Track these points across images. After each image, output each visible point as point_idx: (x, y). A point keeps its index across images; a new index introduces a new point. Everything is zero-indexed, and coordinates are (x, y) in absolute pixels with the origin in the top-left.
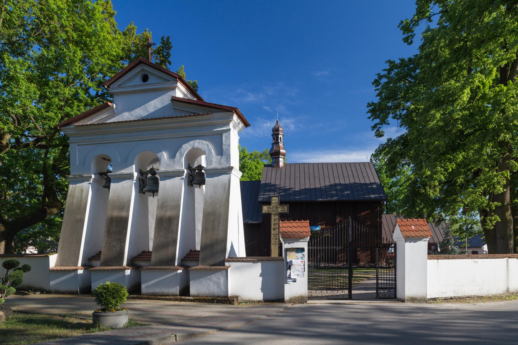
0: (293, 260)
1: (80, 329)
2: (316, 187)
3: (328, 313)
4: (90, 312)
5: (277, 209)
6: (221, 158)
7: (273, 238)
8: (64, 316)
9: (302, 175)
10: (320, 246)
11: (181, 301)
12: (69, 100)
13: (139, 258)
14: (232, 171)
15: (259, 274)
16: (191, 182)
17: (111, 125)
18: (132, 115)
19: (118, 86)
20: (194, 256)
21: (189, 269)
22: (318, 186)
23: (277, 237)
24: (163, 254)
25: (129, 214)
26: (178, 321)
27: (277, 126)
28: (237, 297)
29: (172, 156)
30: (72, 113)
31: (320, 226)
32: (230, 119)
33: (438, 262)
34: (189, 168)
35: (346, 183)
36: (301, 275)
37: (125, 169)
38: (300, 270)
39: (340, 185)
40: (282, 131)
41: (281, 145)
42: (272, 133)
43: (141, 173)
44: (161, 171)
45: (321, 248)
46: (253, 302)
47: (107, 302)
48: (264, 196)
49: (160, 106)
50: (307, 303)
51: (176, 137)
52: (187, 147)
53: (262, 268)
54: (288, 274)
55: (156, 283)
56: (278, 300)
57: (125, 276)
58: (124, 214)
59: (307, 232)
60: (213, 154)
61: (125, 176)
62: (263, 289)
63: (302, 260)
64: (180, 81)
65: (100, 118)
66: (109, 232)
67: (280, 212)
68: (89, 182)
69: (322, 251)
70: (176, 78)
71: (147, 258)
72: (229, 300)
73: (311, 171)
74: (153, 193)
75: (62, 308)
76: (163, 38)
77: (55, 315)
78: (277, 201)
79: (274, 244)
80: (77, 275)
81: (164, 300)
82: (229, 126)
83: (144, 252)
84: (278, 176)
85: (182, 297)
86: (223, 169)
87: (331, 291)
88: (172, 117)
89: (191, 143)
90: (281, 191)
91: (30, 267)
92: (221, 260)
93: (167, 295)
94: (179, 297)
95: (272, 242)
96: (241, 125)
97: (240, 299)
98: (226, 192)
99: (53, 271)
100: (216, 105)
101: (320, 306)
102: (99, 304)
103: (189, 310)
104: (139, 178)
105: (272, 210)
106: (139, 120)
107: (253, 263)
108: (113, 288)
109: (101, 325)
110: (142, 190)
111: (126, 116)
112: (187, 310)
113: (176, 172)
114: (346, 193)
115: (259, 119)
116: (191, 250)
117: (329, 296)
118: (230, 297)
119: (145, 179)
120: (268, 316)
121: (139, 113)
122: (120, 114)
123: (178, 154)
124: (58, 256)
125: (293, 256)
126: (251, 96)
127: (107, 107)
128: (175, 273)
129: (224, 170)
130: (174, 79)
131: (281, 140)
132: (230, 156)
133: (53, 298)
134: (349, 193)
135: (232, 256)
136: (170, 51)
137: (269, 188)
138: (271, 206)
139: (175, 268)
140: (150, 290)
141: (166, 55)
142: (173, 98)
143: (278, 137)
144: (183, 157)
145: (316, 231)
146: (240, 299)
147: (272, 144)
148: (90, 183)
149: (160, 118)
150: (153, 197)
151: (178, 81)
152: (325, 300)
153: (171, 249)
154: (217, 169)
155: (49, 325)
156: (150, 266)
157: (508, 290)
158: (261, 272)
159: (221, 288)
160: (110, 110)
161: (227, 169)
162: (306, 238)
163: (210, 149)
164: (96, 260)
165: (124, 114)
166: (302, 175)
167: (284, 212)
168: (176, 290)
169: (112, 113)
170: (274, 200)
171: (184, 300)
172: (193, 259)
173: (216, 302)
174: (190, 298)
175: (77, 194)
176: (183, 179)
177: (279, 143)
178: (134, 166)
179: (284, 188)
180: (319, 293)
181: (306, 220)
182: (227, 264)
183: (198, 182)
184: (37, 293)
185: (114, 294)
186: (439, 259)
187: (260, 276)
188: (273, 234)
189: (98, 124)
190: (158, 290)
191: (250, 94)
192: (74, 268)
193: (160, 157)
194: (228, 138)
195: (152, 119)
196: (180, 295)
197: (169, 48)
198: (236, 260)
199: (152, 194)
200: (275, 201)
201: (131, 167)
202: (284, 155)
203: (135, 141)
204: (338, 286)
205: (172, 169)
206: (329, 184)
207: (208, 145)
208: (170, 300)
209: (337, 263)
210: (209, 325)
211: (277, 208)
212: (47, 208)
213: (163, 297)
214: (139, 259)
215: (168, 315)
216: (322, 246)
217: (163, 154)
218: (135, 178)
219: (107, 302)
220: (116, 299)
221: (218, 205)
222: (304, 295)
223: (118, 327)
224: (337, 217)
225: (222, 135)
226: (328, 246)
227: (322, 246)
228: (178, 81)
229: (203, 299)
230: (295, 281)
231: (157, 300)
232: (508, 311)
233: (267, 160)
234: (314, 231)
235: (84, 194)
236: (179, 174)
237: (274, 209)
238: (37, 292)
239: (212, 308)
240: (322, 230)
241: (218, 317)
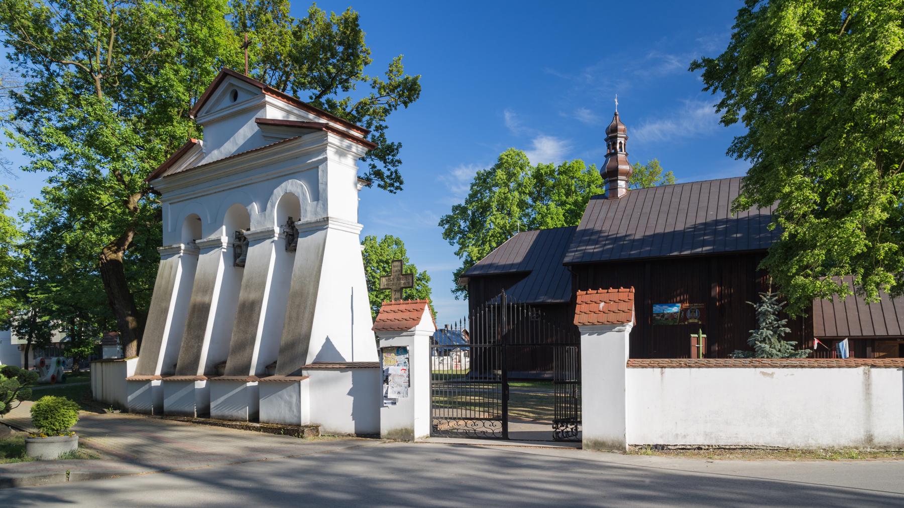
5: (398, 282)
6: (317, 204)
18: (221, 153)
19: (206, 113)
31: (679, 305)
33: (662, 373)
36: (403, 393)
37: (214, 234)
49: (249, 135)
50: (414, 442)
52: (279, 193)
55: (226, 401)
57: (194, 389)
58: (206, 299)
62: (355, 416)
63: (405, 368)
64: (269, 93)
65: (188, 163)
68: (178, 255)
80: (151, 388)
84: (611, 214)
89: (283, 185)
104: (234, 245)
105: (393, 284)
111: (216, 155)
114: (739, 235)
115: (687, 102)
121: (229, 148)
123: (269, 205)
124: (139, 361)
126: (673, 61)
127: (193, 146)
128: (244, 386)
131: (621, 148)
143: (615, 144)
145: (672, 313)
157: (870, 439)
158: (351, 386)
165: (213, 152)
166: (656, 208)
168: (245, 412)
173: (284, 434)
174: (258, 425)
178: (224, 227)
184: (115, 412)
186: (665, 367)
187: (350, 394)
191: (671, 57)
193: (251, 210)
196: (250, 421)
203: (226, 190)
207: (302, 186)
217: (253, 207)
218: (225, 245)
232: (736, 478)
234: (668, 314)
237: (396, 280)
240: (684, 311)
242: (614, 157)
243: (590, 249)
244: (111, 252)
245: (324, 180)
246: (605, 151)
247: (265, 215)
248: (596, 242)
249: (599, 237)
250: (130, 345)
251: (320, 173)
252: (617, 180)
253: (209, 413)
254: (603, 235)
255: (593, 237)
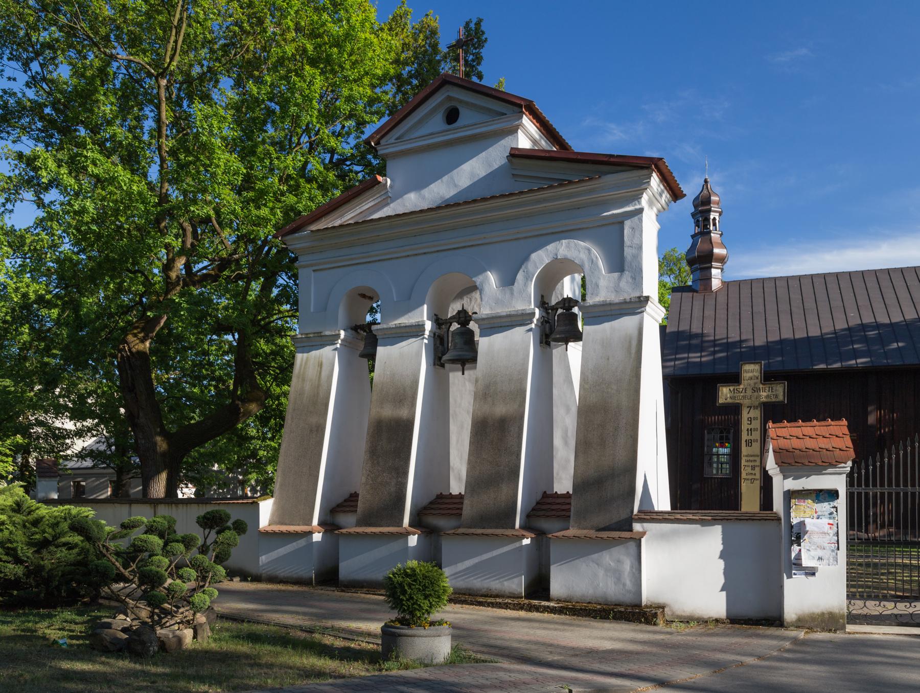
0: (808, 521)
1: (358, 661)
2: (810, 335)
3: (904, 658)
4: (376, 627)
5: (756, 394)
6: (620, 278)
7: (746, 464)
8: (311, 631)
9: (771, 306)
10: (875, 485)
11: (530, 611)
12: (292, 178)
13: (432, 509)
14: (647, 308)
15: (718, 554)
16: (547, 336)
17: (381, 222)
18: (424, 198)
20: (451, 506)
21: (550, 536)
22: (814, 332)
23: (758, 463)
24: (488, 500)
25: (415, 413)
26: (550, 658)
27: (705, 192)
28: (662, 607)
29: (508, 281)
30: (300, 207)
32: (643, 187)
34: (543, 304)
35: (893, 321)
37: (406, 316)
38: (826, 545)
39: (877, 326)
40: (718, 204)
41: (715, 236)
42: (693, 210)
43: (439, 322)
44: (484, 317)
45: (878, 490)
46: (703, 622)
47: (413, 604)
48: (677, 363)
50: (845, 633)
51: (515, 237)
52: (541, 259)
53: (723, 539)
54: (793, 555)
55: (475, 567)
56: (765, 620)
57: (407, 548)
58: (404, 413)
59: (844, 448)
60: (600, 270)
61: (408, 330)
63: (831, 521)
64: (527, 113)
65: (359, 211)
66: (373, 452)
67: (764, 400)
69: (890, 500)
70: (520, 106)
71: (449, 509)
72: (645, 613)
73: (796, 296)
74: (463, 365)
75: (297, 613)
76: (467, 24)
77: (293, 627)
78: (757, 374)
79: (748, 479)
80: (311, 544)
81: (493, 607)
82: (640, 203)
83: (440, 497)
84: (709, 312)
85: (532, 601)
86: (625, 302)
87: (908, 604)
88: (511, 194)
89: (551, 247)
90: (716, 349)
91: (246, 524)
92: (624, 515)
93: (497, 596)
94: (526, 601)
95: (744, 475)
96: (666, 196)
97: (669, 613)
98: (633, 356)
99: (266, 534)
100: (612, 156)
101: (881, 641)
102: (393, 608)
103: (559, 633)
104: (434, 334)
105: (744, 397)
106: (439, 208)
107: (703, 526)
108: (423, 575)
109: (401, 655)
110: (440, 359)
111: (412, 201)
112: (555, 633)
113: (516, 316)
114: (895, 345)
116: (545, 492)
117: (901, 615)
118: (646, 606)
119: (446, 336)
120: (760, 657)
122: (398, 199)
123: (520, 276)
124: (275, 503)
125: (808, 510)
128: (517, 545)
129: (624, 306)
130: (516, 109)
131: (714, 225)
132: (642, 271)
133: (268, 591)
134: (903, 347)
135: (645, 508)
136: (481, 50)
137: (687, 342)
138: (742, 386)
139: (515, 533)
140: (461, 583)
141: (473, 60)
142: (513, 153)
143: (707, 219)
144: (531, 281)
146: (669, 613)
147: (693, 237)
148: (336, 349)
149: (484, 199)
150: (463, 374)
151: (524, 113)
152: (890, 625)
153: (505, 489)
154: (610, 304)
155: (294, 648)
156: (459, 527)
158: (721, 547)
159: (624, 585)
160: (380, 192)
161: (635, 302)
162: (843, 465)
163: (595, 259)
164: (345, 512)
166: (771, 306)
167: (774, 400)
168: (518, 584)
169: (384, 197)
170: (747, 372)
171: (537, 609)
172: (554, 513)
175: (311, 373)
176: (530, 330)
177: (710, 232)
178: (425, 306)
179: (725, 341)
180: (873, 607)
181: (839, 419)
182: (637, 527)
183: (563, 336)
185: (427, 587)
188: (747, 456)
189: (356, 223)
190: (478, 583)
191: (612, 126)
192: (305, 528)
193: (482, 283)
194: (638, 230)
195: (466, 203)
197: (481, 43)
198: (661, 517)
199: (459, 366)
200: (751, 375)
201: (417, 311)
202: (722, 260)
203: (428, 253)
204: (904, 590)
205: (507, 310)
206: (846, 326)
207: (589, 250)
208: (506, 606)
209: (871, 527)
210: (627, 672)
211: (756, 390)
212: (240, 403)
213: (489, 600)
214: (433, 512)
215: (520, 641)
216: (882, 485)
217: (487, 278)
218: (427, 333)
219: (413, 604)
220: (431, 600)
221: (615, 387)
222: (836, 611)
223: (435, 662)
224: (870, 409)
225: (622, 223)
226: (898, 485)
227: (882, 485)
228: (524, 113)
229: (581, 609)
230: (811, 572)
231: (476, 605)
233: (672, 276)
235: (324, 373)
236: (522, 319)
237: (749, 392)
238: (234, 577)
239: (609, 630)
241: (638, 653)
242: (706, 237)
243: (695, 357)
244: (138, 341)
245: (636, 241)
246: (692, 229)
247: (512, 290)
248: (700, 348)
249: (702, 342)
250: (156, 479)
251: (627, 231)
252: (711, 267)
253: (547, 589)
254: (707, 339)
255: (694, 342)
